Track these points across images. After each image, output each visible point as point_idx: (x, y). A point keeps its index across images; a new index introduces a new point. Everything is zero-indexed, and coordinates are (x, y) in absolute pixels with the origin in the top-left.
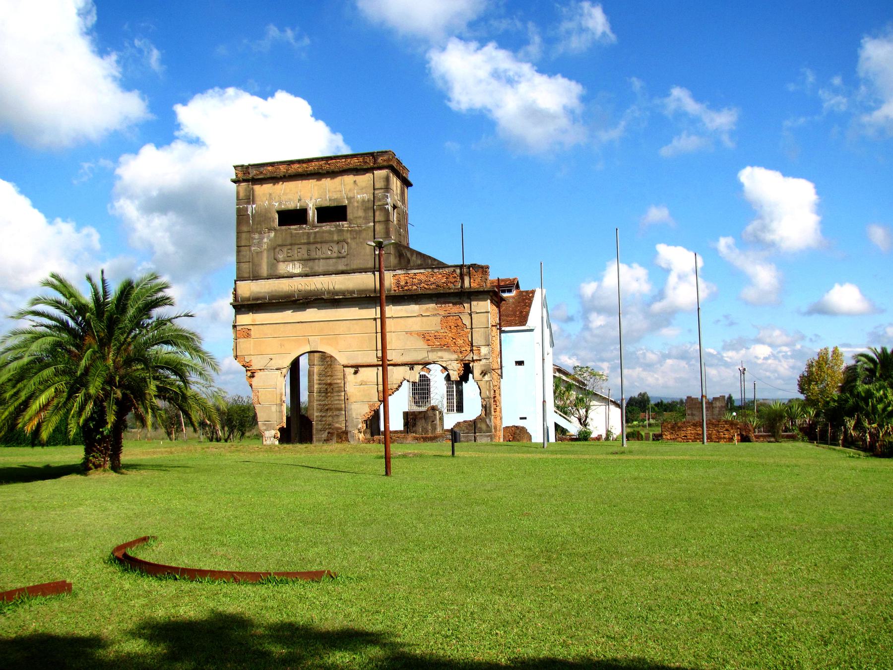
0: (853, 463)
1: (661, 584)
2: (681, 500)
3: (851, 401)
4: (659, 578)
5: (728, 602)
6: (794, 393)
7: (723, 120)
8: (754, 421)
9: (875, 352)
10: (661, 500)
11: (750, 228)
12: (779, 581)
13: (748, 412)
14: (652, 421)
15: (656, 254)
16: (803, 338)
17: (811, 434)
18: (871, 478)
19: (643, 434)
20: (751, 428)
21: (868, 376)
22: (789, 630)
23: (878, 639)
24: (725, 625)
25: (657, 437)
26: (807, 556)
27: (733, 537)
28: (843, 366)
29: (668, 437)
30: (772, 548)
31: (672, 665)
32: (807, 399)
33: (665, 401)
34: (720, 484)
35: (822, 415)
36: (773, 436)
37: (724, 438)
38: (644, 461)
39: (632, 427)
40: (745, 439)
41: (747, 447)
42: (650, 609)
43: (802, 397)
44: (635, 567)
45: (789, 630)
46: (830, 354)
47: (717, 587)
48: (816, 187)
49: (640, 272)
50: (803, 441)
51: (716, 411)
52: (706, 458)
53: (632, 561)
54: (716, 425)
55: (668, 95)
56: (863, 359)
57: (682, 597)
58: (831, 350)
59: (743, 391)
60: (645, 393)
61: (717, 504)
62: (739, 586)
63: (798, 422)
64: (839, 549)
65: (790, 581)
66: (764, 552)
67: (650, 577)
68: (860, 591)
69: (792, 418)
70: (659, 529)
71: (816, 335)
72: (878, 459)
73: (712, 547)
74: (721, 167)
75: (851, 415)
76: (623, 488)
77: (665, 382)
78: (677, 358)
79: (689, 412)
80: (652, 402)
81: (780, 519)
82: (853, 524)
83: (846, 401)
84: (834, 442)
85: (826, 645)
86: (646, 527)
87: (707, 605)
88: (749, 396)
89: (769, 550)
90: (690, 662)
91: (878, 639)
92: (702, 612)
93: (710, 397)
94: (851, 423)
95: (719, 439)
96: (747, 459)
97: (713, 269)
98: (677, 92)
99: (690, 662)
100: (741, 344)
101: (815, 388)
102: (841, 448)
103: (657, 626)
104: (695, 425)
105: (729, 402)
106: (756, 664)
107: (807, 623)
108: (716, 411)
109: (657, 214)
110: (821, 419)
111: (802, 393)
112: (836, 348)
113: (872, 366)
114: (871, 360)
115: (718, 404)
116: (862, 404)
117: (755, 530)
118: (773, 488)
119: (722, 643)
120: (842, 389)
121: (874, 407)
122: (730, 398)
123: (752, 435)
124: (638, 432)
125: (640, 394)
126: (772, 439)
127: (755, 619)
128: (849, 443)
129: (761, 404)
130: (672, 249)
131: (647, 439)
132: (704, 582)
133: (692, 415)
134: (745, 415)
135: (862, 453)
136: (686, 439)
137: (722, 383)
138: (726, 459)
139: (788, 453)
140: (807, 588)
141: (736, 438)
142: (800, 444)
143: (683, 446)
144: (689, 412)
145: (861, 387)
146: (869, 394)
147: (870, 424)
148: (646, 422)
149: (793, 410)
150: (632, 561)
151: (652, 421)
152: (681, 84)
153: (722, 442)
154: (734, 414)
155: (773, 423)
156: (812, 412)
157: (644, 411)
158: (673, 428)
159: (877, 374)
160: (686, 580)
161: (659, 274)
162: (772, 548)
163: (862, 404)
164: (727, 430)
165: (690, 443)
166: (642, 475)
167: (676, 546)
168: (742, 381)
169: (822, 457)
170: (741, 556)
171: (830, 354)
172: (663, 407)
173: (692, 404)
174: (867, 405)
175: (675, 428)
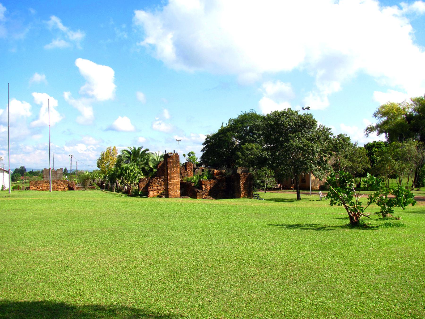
0: (118, 199)
1: (21, 261)
2: (36, 219)
3: (119, 171)
4: (21, 258)
5: (54, 267)
6: (94, 167)
7: (78, 36)
8: (76, 180)
9: (131, 149)
10: (26, 220)
11: (83, 88)
12: (79, 255)
13: (74, 176)
14: (27, 181)
15: (33, 98)
16: (103, 142)
17: (102, 186)
18: (125, 206)
19: (21, 187)
20: (74, 183)
21: (127, 160)
22: (80, 277)
23: (119, 277)
24: (51, 278)
25: (28, 189)
26: (93, 243)
27: (60, 236)
28: (117, 155)
29: (33, 188)
30: (77, 240)
31: (23, 300)
32: (101, 170)
33: (34, 171)
34: (57, 210)
35: (107, 177)
36: (84, 187)
37: (61, 189)
38: (19, 200)
39: (17, 183)
40: (71, 189)
41: (71, 193)
42: (14, 274)
43: (99, 169)
44: (8, 254)
45: (80, 277)
46: (112, 149)
47: (49, 260)
48: (115, 74)
49: (28, 106)
50: (98, 189)
51: (58, 176)
52: (51, 198)
53: (7, 251)
54: (57, 183)
55: (50, 19)
56: (126, 152)
57: (31, 267)
58: (112, 148)
59: (71, 166)
60: (23, 167)
61: (54, 220)
62: (60, 259)
63: (97, 181)
64: (108, 239)
65: (84, 255)
66: (74, 242)
67: (16, 258)
68: (115, 257)
69: (94, 180)
70: (23, 234)
71: (109, 141)
72: (129, 197)
73: (49, 241)
74: (68, 58)
75: (119, 177)
76: (7, 214)
77: (34, 162)
78: (42, 150)
79: (45, 176)
80: (27, 171)
81: (83, 226)
82: (115, 227)
83: (117, 171)
84: (111, 190)
85: (97, 282)
86: (17, 233)
87: (43, 269)
88: (74, 168)
89: (76, 241)
90: (31, 298)
91: (119, 277)
92: (40, 273)
93: (55, 169)
94: (119, 181)
95: (58, 189)
96: (70, 199)
97: (63, 107)
98: (54, 19)
99: (31, 298)
100: (73, 143)
101: (104, 166)
102: (114, 192)
103: (17, 282)
104: (46, 182)
105: (65, 172)
106: (64, 295)
107: (90, 273)
108: (58, 176)
109: (38, 77)
110: (106, 179)
111: (98, 167)
112: (115, 147)
113: (129, 155)
114: (129, 153)
115: (59, 172)
116: (124, 173)
117: (70, 232)
118: (81, 212)
119: (49, 287)
120: (116, 166)
121: (129, 174)
122: (66, 169)
123: (75, 187)
124: (19, 186)
125: (21, 167)
126: (84, 189)
127: (66, 274)
128: (119, 190)
129: (80, 172)
130: (40, 94)
131: (23, 190)
132: (43, 258)
133: (47, 177)
134: (72, 178)
135: (123, 195)
136: (42, 189)
137: (61, 162)
138: (60, 199)
139: (90, 195)
140: (91, 257)
141: (66, 189)
142: (96, 191)
143: (40, 192)
144: (45, 176)
145: (124, 165)
146: (127, 168)
147: (127, 181)
148: (24, 181)
149: (94, 175)
150: (7, 251)
151: (27, 181)
152: (57, 15)
153: (60, 191)
154: (67, 177)
155: (85, 181)
156: (103, 176)
157: (23, 176)
158: (35, 184)
159: (131, 159)
160: (34, 258)
161: (36, 107)
162: (77, 240)
163: (124, 173)
164: (62, 185)
165: (44, 191)
166: (17, 207)
167: (31, 242)
168: (71, 161)
169: (105, 197)
170: (62, 245)
171: (112, 149)
172: (32, 173)
173: (45, 172)
174: (126, 173)
175: (37, 184)
